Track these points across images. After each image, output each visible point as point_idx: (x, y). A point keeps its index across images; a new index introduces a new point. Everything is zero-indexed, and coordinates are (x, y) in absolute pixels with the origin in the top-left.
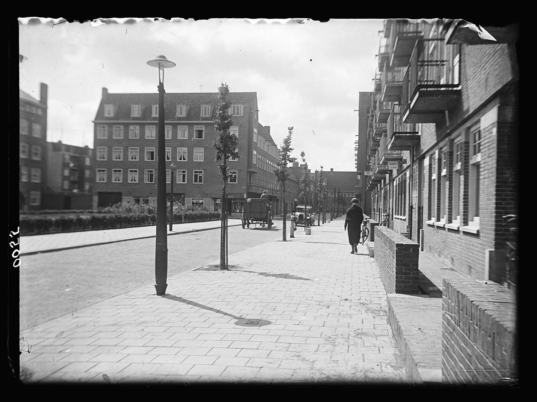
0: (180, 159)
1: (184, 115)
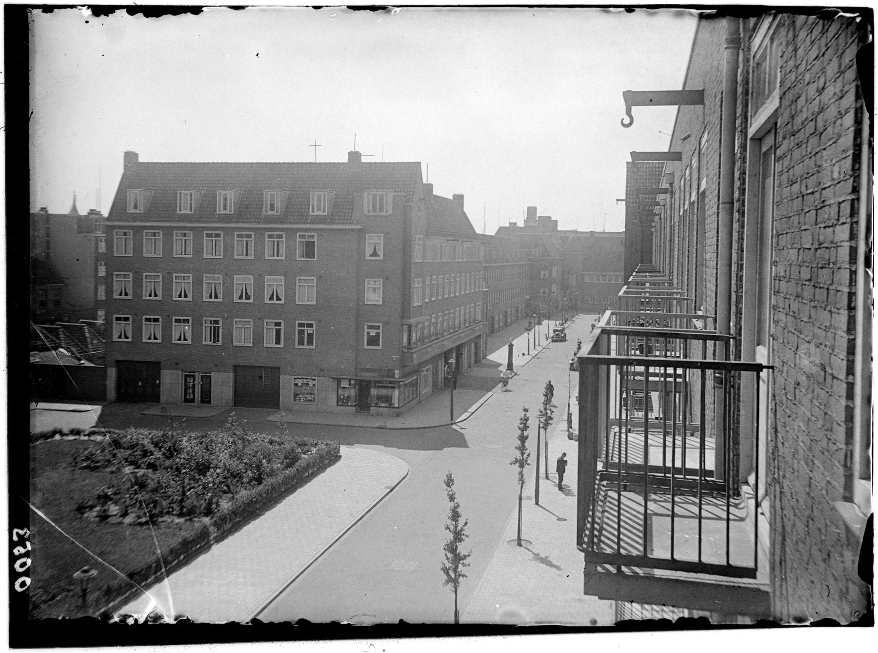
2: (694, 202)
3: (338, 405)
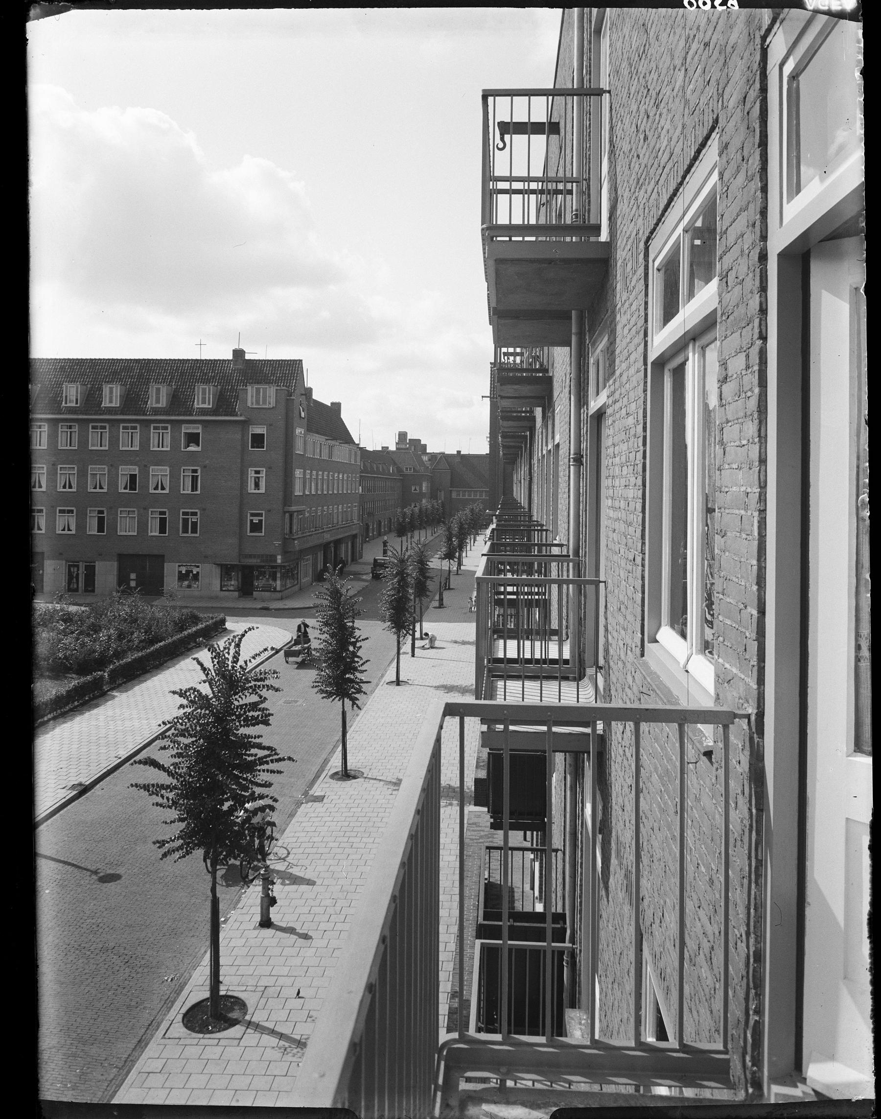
0: (156, 488)
1: (163, 403)
2: (550, 451)
3: (221, 590)
